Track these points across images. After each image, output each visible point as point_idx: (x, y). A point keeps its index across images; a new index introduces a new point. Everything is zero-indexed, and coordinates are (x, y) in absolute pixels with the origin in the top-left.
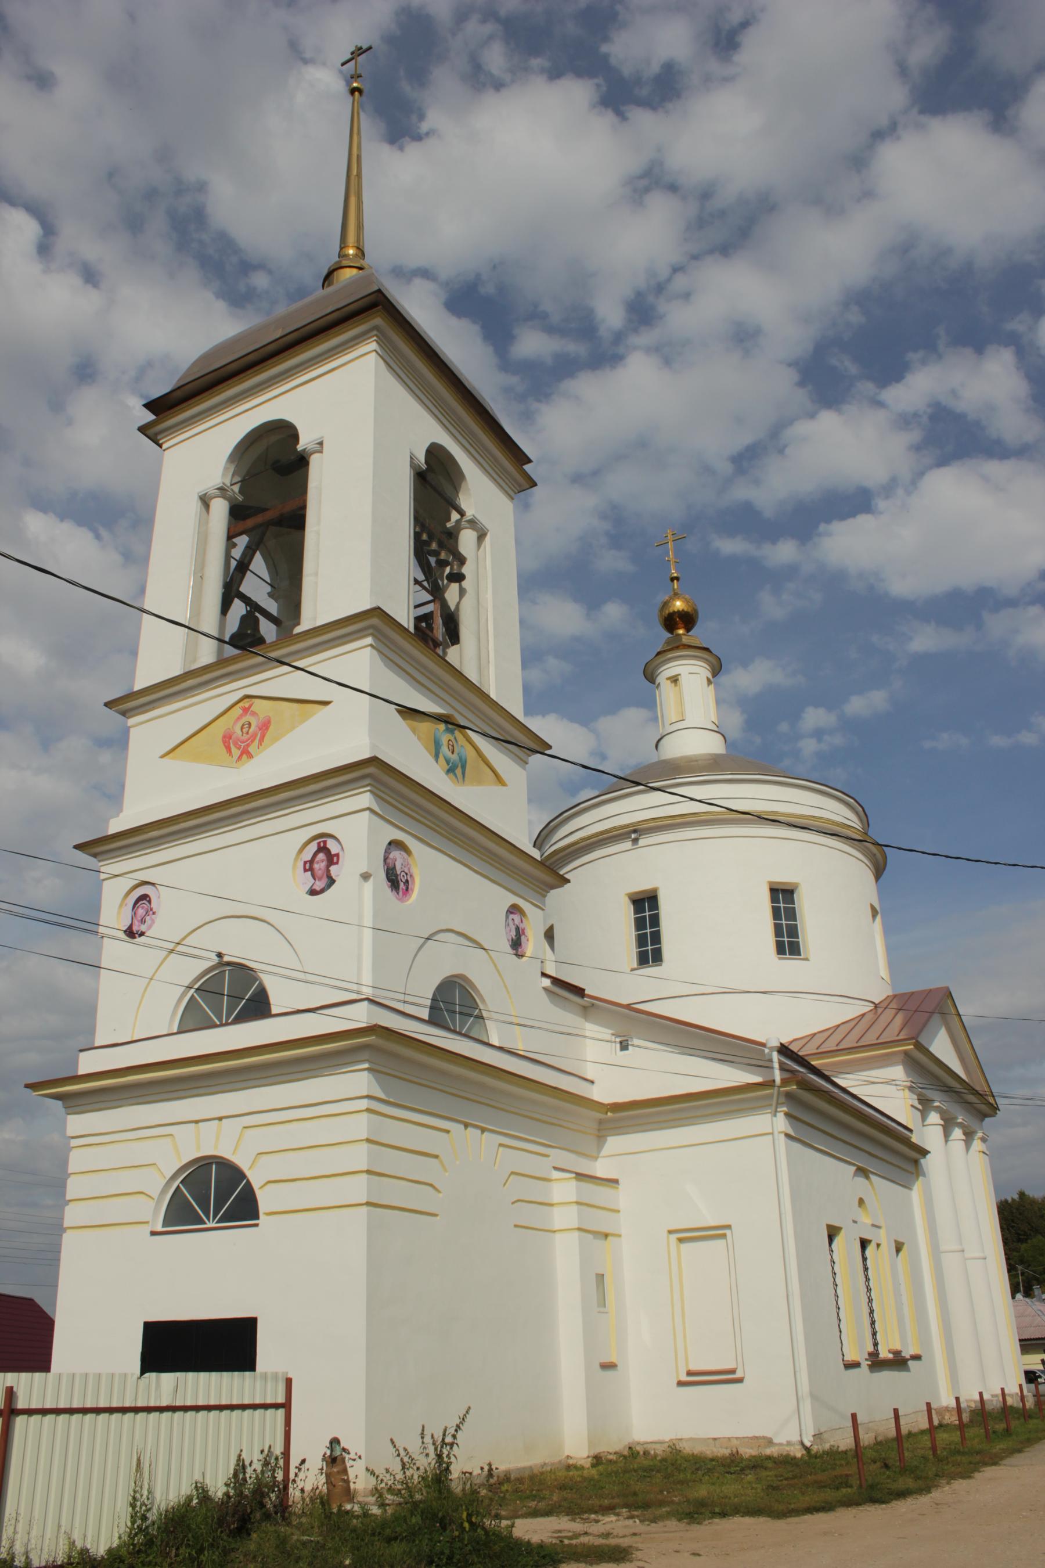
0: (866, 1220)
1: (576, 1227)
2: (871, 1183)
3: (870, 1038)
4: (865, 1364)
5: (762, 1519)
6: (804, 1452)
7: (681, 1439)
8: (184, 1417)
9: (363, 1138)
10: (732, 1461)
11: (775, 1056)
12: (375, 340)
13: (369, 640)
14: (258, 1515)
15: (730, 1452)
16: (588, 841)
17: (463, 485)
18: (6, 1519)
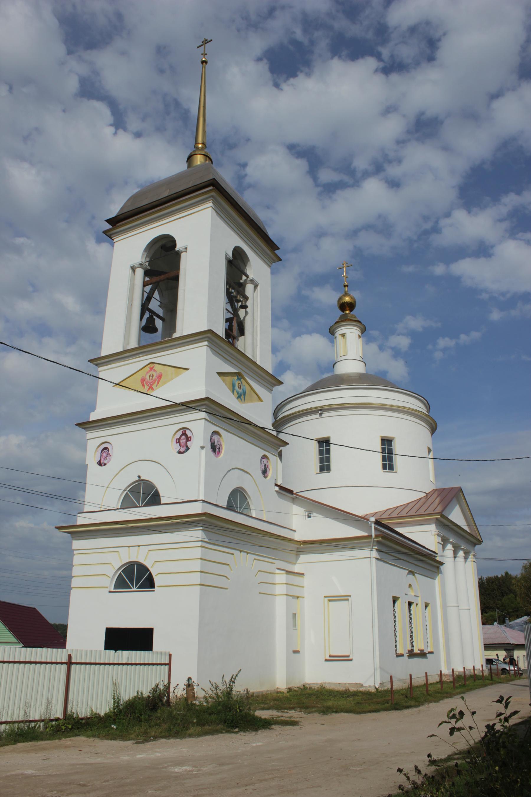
0: (411, 593)
1: (285, 594)
2: (415, 577)
3: (421, 512)
4: (406, 655)
5: (351, 714)
6: (375, 690)
7: (325, 683)
8: (3, 665)
9: (199, 558)
10: (345, 693)
11: (373, 525)
12: (212, 202)
13: (206, 343)
14: (160, 704)
15: (345, 689)
16: (299, 413)
17: (248, 263)
18: (69, 701)
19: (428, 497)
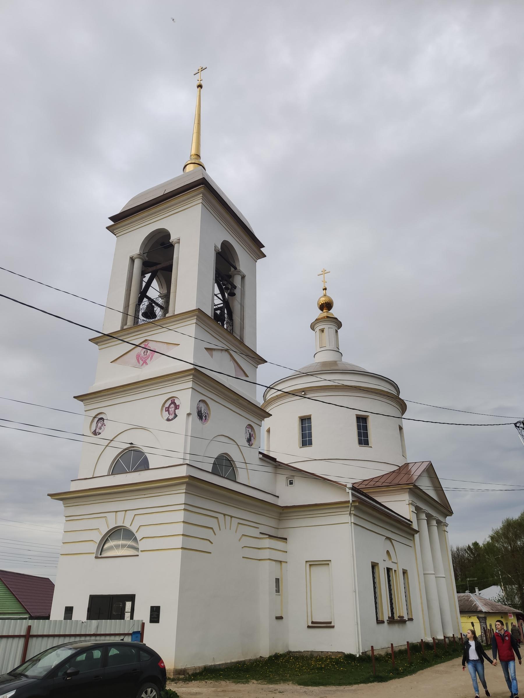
11: (350, 491)
19: (401, 470)
